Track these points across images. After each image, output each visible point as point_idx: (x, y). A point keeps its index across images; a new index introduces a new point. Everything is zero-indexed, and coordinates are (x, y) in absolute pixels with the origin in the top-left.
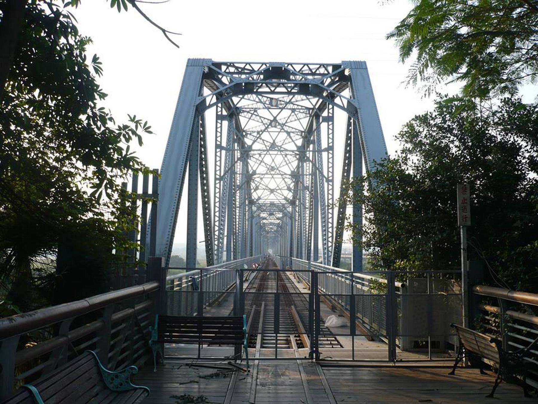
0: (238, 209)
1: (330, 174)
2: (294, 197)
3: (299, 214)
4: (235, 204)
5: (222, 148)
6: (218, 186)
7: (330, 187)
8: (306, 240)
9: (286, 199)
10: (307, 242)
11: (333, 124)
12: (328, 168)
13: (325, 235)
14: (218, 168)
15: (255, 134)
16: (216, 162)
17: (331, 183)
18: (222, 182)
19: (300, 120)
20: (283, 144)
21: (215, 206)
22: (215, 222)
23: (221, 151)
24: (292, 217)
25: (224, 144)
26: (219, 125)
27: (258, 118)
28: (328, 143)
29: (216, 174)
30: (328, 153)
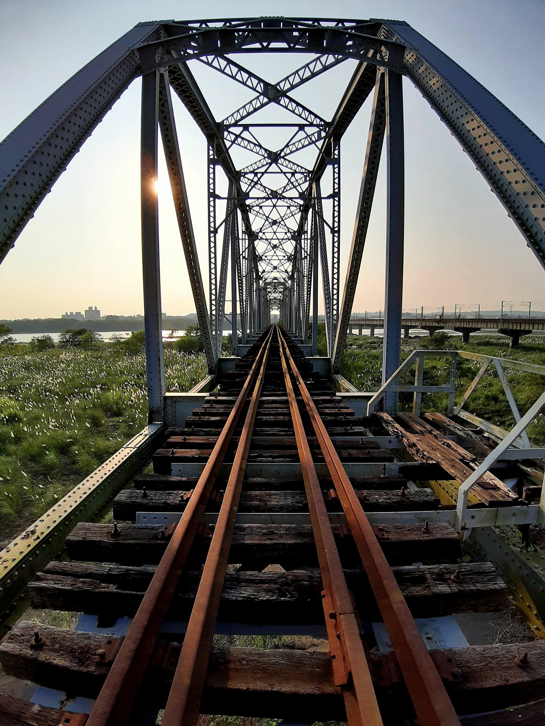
1: (336, 225)
3: (297, 284)
9: (286, 271)
20: (283, 192)
24: (291, 290)
26: (211, 171)
28: (334, 189)
30: (334, 200)
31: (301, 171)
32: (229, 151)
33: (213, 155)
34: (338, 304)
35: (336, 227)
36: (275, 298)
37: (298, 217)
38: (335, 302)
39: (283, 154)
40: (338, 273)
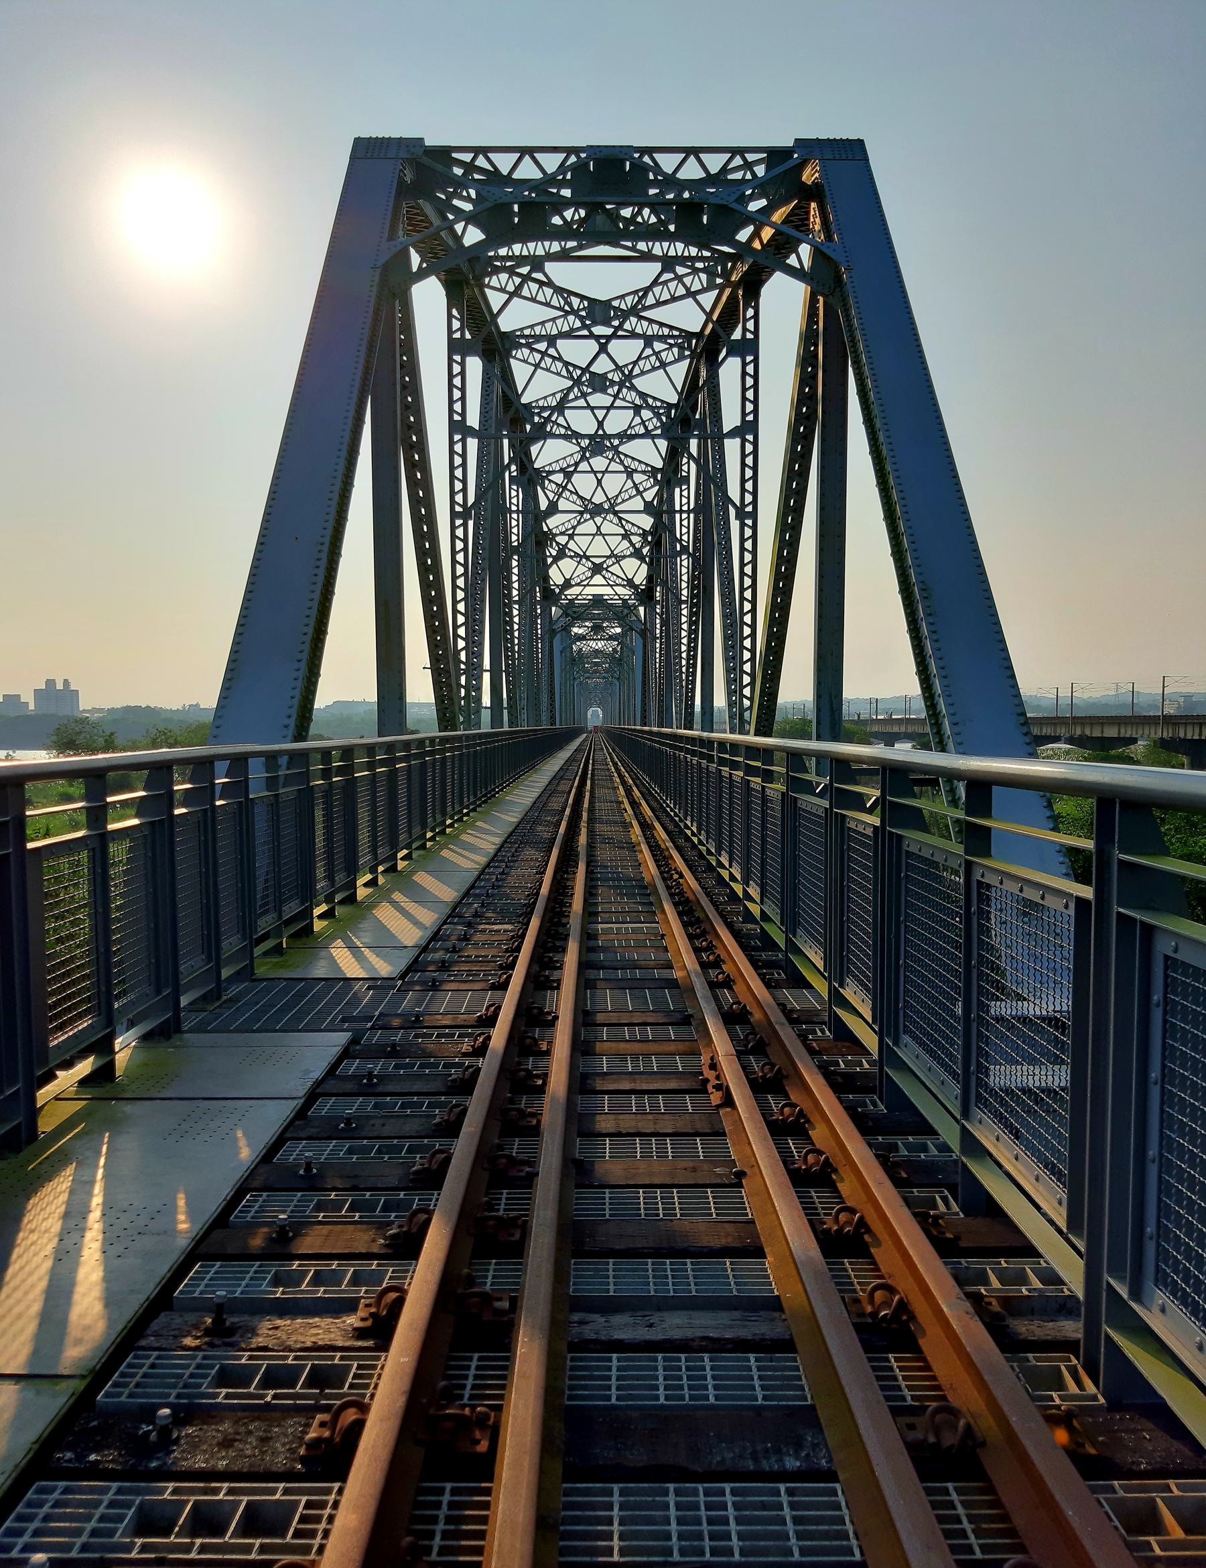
0: (517, 606)
2: (650, 578)
4: (510, 596)
5: (467, 431)
6: (460, 532)
7: (748, 532)
8: (681, 696)
9: (630, 583)
11: (756, 362)
12: (743, 481)
13: (734, 669)
14: (458, 486)
15: (558, 478)
16: (452, 468)
17: (749, 522)
18: (471, 523)
21: (455, 587)
22: (456, 627)
23: (464, 441)
24: (646, 632)
25: (473, 420)
27: (549, 291)
28: (744, 414)
29: (453, 502)
32: (499, 320)
33: (461, 329)
34: (753, 635)
35: (749, 413)
36: (597, 652)
38: (747, 631)
39: (605, 566)
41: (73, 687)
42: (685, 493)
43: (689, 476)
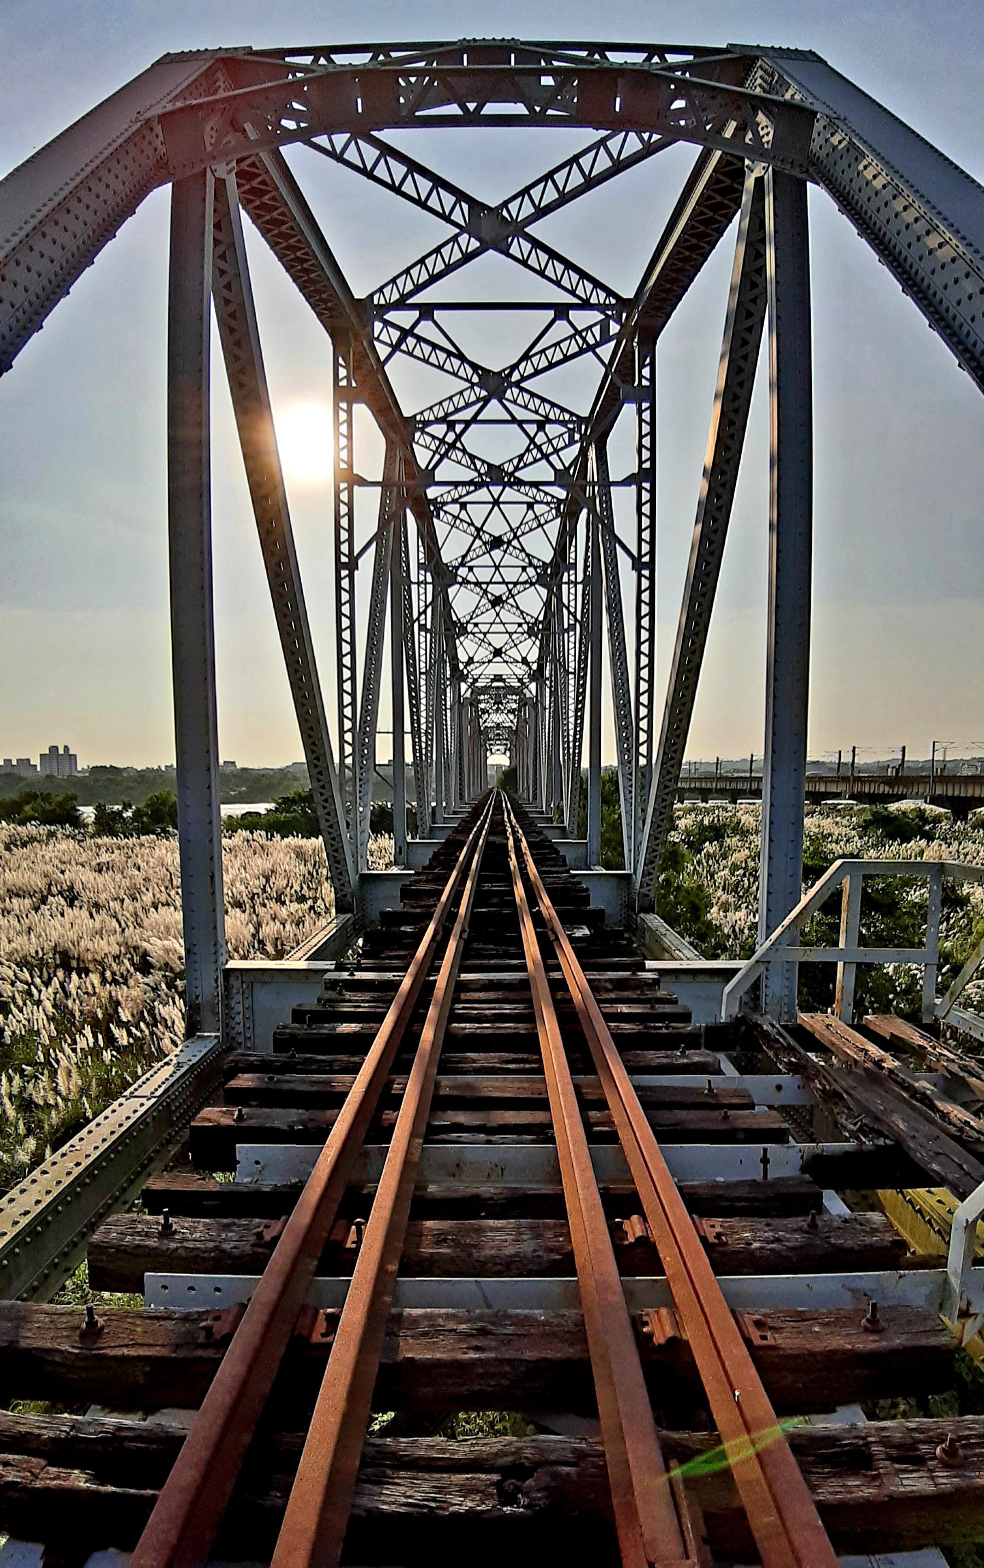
3: (551, 691)
9: (525, 661)
10: (571, 751)
12: (639, 643)
16: (341, 681)
17: (646, 572)
19: (573, 332)
21: (342, 741)
24: (536, 704)
28: (641, 462)
31: (561, 418)
33: (348, 378)
37: (553, 528)
38: (643, 737)
40: (651, 665)
41: (71, 752)
42: (572, 639)
43: (575, 563)
